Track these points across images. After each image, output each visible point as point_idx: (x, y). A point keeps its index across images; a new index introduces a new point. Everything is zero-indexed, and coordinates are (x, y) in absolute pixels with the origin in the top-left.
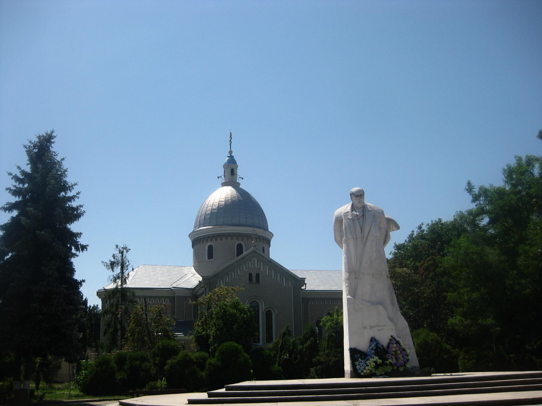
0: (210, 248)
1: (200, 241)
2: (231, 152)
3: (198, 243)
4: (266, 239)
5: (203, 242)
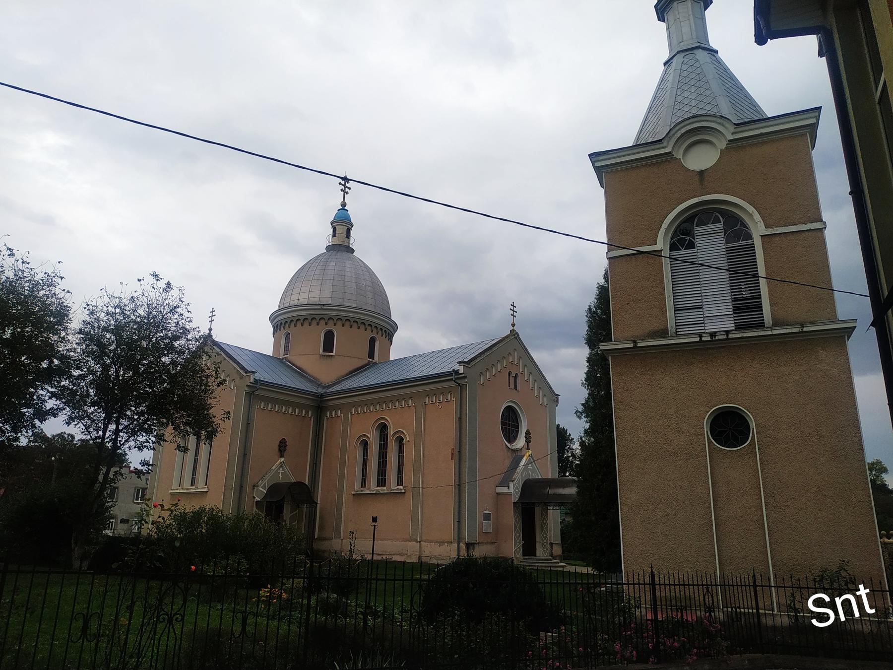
1: (280, 327)
2: (344, 204)
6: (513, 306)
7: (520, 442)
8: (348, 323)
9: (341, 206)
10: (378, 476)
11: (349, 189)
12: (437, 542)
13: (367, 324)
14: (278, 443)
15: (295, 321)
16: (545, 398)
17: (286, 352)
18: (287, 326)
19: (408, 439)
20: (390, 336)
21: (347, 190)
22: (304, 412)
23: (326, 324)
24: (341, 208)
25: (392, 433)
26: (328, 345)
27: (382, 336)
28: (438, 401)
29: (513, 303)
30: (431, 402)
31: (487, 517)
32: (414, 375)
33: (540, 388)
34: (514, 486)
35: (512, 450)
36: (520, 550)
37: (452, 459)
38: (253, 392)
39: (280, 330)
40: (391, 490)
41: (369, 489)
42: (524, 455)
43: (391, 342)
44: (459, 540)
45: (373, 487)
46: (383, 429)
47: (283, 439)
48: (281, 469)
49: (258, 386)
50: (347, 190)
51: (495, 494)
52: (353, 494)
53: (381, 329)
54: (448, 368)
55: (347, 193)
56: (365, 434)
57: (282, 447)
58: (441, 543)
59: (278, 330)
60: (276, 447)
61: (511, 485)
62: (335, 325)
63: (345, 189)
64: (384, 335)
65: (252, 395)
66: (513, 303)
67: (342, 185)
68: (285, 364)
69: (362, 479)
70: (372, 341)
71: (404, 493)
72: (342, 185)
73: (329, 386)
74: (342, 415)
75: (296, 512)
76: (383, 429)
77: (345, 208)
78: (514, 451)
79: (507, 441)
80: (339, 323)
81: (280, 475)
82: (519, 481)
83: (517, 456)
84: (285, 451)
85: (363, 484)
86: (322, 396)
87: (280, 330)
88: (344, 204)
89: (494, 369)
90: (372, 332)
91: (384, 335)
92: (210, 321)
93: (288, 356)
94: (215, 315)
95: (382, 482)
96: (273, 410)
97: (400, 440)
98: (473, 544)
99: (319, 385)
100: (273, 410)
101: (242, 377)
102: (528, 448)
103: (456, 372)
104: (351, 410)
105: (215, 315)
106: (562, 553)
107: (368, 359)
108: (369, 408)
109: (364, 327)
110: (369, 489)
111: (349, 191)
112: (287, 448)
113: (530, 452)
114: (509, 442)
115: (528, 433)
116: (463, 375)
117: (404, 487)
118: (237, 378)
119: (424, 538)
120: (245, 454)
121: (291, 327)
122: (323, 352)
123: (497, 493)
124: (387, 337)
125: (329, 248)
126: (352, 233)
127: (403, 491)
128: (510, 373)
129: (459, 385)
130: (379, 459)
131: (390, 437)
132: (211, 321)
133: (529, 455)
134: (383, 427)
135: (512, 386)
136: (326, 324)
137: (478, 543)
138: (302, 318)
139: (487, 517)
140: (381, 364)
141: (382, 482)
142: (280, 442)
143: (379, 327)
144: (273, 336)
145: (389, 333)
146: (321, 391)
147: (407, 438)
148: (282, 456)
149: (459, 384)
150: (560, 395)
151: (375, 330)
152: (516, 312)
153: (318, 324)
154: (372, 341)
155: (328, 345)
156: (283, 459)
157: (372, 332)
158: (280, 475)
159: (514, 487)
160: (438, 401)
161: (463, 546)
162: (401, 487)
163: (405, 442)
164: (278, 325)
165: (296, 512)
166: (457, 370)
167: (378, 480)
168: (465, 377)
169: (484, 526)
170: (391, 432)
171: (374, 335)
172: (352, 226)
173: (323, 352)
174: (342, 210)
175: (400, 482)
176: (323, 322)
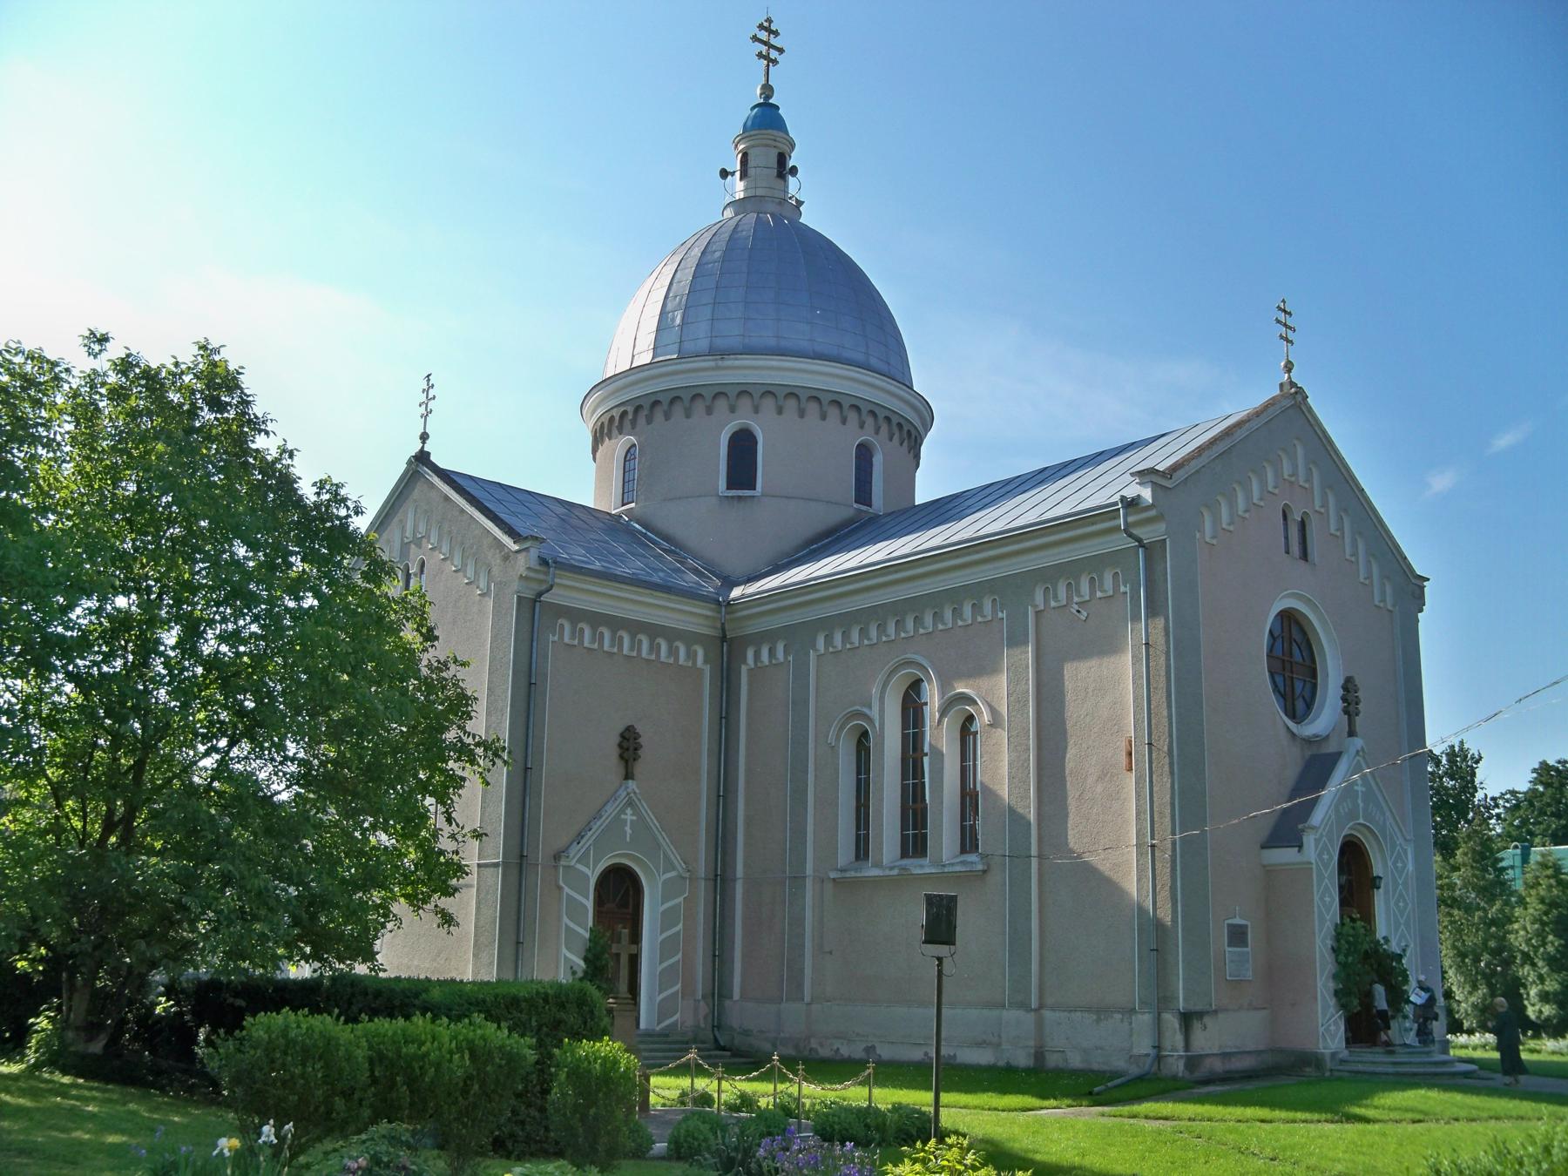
0: (743, 448)
2: (768, 90)
3: (615, 432)
7: (1326, 718)
8: (792, 403)
10: (904, 827)
12: (1089, 1010)
13: (846, 405)
14: (617, 740)
23: (733, 409)
27: (891, 439)
31: (1238, 936)
34: (1317, 841)
35: (1304, 739)
36: (1338, 1029)
38: (540, 594)
40: (944, 866)
43: (917, 457)
44: (1161, 1001)
48: (629, 811)
50: (774, 54)
52: (834, 879)
56: (858, 708)
58: (1101, 1011)
60: (614, 752)
62: (756, 410)
64: (896, 437)
65: (538, 604)
66: (1284, 301)
69: (858, 836)
70: (864, 454)
71: (984, 872)
74: (790, 658)
77: (771, 101)
78: (1308, 741)
80: (768, 404)
81: (1359, 801)
88: (768, 90)
91: (896, 437)
98: (1200, 1015)
103: (1131, 504)
106: (1378, 1011)
107: (855, 506)
110: (878, 865)
114: (1293, 716)
115: (1349, 687)
116: (1153, 513)
117: (984, 857)
118: (495, 560)
119: (1049, 1001)
120: (526, 769)
122: (728, 489)
123: (1264, 866)
124: (905, 444)
127: (980, 867)
129: (1141, 544)
130: (903, 780)
132: (425, 417)
133: (1358, 752)
134: (910, 687)
136: (733, 409)
137: (1216, 1012)
138: (665, 399)
140: (889, 519)
142: (622, 736)
145: (909, 431)
149: (1139, 540)
150: (1428, 580)
151: (870, 421)
158: (1359, 801)
159: (1316, 847)
161: (1171, 1021)
162: (972, 858)
163: (977, 726)
167: (904, 839)
169: (1232, 961)
171: (866, 436)
172: (792, 146)
173: (728, 489)
176: (722, 404)
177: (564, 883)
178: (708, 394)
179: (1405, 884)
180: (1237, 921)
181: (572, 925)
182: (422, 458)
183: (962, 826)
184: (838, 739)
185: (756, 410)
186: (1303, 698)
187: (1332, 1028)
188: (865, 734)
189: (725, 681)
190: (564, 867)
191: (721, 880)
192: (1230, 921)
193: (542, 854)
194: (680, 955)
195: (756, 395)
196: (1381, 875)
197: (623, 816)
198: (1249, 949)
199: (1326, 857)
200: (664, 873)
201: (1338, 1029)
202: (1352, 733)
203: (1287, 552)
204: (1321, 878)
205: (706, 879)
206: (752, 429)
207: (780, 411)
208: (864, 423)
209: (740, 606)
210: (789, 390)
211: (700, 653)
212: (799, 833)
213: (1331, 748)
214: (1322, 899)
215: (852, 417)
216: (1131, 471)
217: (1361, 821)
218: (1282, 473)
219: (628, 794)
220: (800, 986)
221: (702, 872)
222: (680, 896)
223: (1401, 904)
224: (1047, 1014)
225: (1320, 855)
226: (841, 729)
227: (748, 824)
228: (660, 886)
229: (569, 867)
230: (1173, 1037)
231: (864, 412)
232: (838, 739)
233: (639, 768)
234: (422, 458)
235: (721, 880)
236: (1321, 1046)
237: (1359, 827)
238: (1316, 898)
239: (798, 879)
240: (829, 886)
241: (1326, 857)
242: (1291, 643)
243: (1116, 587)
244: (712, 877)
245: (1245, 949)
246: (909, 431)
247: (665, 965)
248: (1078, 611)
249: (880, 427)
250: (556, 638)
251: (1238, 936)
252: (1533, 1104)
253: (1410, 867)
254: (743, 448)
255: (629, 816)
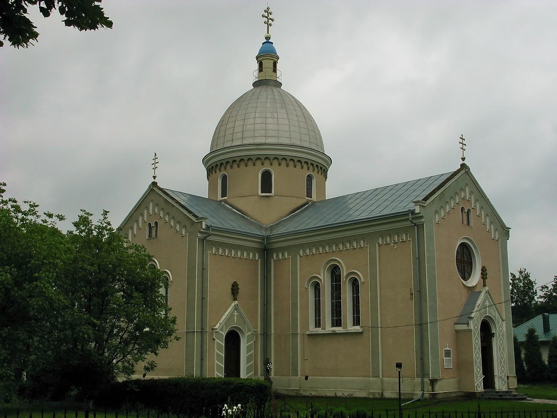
0: (267, 177)
1: (216, 169)
2: (268, 38)
3: (218, 170)
4: (321, 168)
5: (232, 167)
6: (462, 138)
7: (475, 280)
9: (266, 39)
11: (272, 20)
14: (230, 287)
15: (231, 162)
16: (496, 232)
17: (224, 194)
18: (223, 168)
19: (362, 280)
20: (323, 171)
21: (270, 21)
22: (251, 254)
23: (263, 164)
24: (266, 41)
25: (345, 274)
26: (266, 185)
27: (318, 173)
28: (393, 242)
29: (462, 135)
30: (385, 243)
32: (364, 216)
33: (491, 222)
37: (411, 299)
38: (205, 237)
39: (216, 173)
41: (324, 329)
42: (481, 292)
45: (329, 328)
46: (335, 272)
47: (235, 283)
48: (236, 312)
49: (211, 232)
50: (266, 14)
51: (454, 331)
53: (317, 166)
54: (400, 208)
55: (270, 25)
57: (235, 290)
59: (214, 172)
60: (230, 291)
61: (471, 322)
62: (271, 164)
63: (268, 21)
65: (205, 241)
66: (462, 135)
67: (265, 17)
68: (224, 206)
69: (316, 319)
70: (310, 178)
72: (265, 17)
73: (272, 228)
75: (251, 352)
76: (335, 272)
77: (270, 41)
79: (462, 278)
81: (235, 318)
82: (478, 317)
83: (473, 292)
84: (237, 293)
85: (318, 324)
86: (268, 238)
87: (216, 173)
88: (268, 38)
89: (447, 206)
90: (308, 169)
92: (153, 169)
93: (226, 198)
94: (158, 163)
95: (337, 322)
96: (230, 255)
97: (355, 283)
99: (261, 227)
100: (230, 255)
101: (193, 223)
102: (484, 285)
103: (413, 212)
104: (299, 251)
105: (158, 163)
107: (307, 198)
108: (317, 249)
109: (307, 166)
111: (272, 23)
112: (239, 291)
113: (487, 288)
115: (484, 270)
121: (227, 169)
123: (456, 330)
125: (255, 84)
126: (278, 65)
128: (462, 209)
129: (415, 225)
131: (343, 279)
134: (333, 268)
135: (465, 222)
136: (263, 164)
138: (238, 159)
139: (448, 354)
141: (337, 322)
142: (233, 285)
143: (315, 164)
144: (208, 178)
145: (324, 169)
146: (264, 233)
147: (362, 278)
148: (235, 299)
151: (311, 167)
152: (465, 145)
153: (232, 167)
154: (310, 178)
155: (266, 185)
156: (236, 302)
157: (308, 169)
160: (393, 242)
164: (210, 168)
165: (251, 352)
166: (413, 210)
168: (422, 217)
170: (344, 273)
172: (278, 58)
174: (268, 44)
175: (357, 322)
177: (215, 337)
178: (254, 158)
179: (504, 362)
180: (447, 349)
181: (218, 352)
182: (154, 184)
183: (353, 316)
184: (308, 286)
185: (271, 164)
186: (468, 272)
187: (479, 384)
188: (318, 284)
189: (266, 264)
190: (215, 332)
191: (266, 334)
192: (445, 349)
193: (208, 329)
194: (253, 362)
195: (272, 159)
196: (494, 332)
197: (234, 313)
198: (451, 358)
199: (476, 327)
200: (247, 333)
201: (481, 385)
202: (484, 285)
203: (463, 223)
204: (475, 334)
205: (261, 334)
206: (270, 171)
207: (280, 165)
208: (309, 168)
209: (271, 239)
210: (283, 157)
211: (257, 255)
212: (295, 319)
213: (477, 290)
214: (475, 341)
215: (305, 166)
216: (413, 201)
217: (488, 315)
218: (461, 196)
219: (235, 305)
220: (297, 371)
221: (259, 332)
222: (252, 341)
223: (502, 356)
224: (385, 379)
225: (474, 327)
226: (310, 282)
227: (275, 315)
228: (246, 336)
229: (217, 332)
230: (428, 387)
231: (309, 164)
232: (308, 286)
233: (239, 296)
234: (154, 184)
235: (266, 334)
236: (476, 390)
237: (487, 317)
238: (473, 341)
239: (295, 335)
240: (306, 337)
241: (476, 327)
242: (464, 254)
243: (407, 238)
244: (263, 333)
245: (450, 358)
246: (324, 169)
247: (248, 365)
248: (394, 246)
249: (314, 169)
250: (210, 252)
251: (448, 354)
252: (306, 395)
253: (504, 329)
254: (267, 177)
255: (236, 313)
